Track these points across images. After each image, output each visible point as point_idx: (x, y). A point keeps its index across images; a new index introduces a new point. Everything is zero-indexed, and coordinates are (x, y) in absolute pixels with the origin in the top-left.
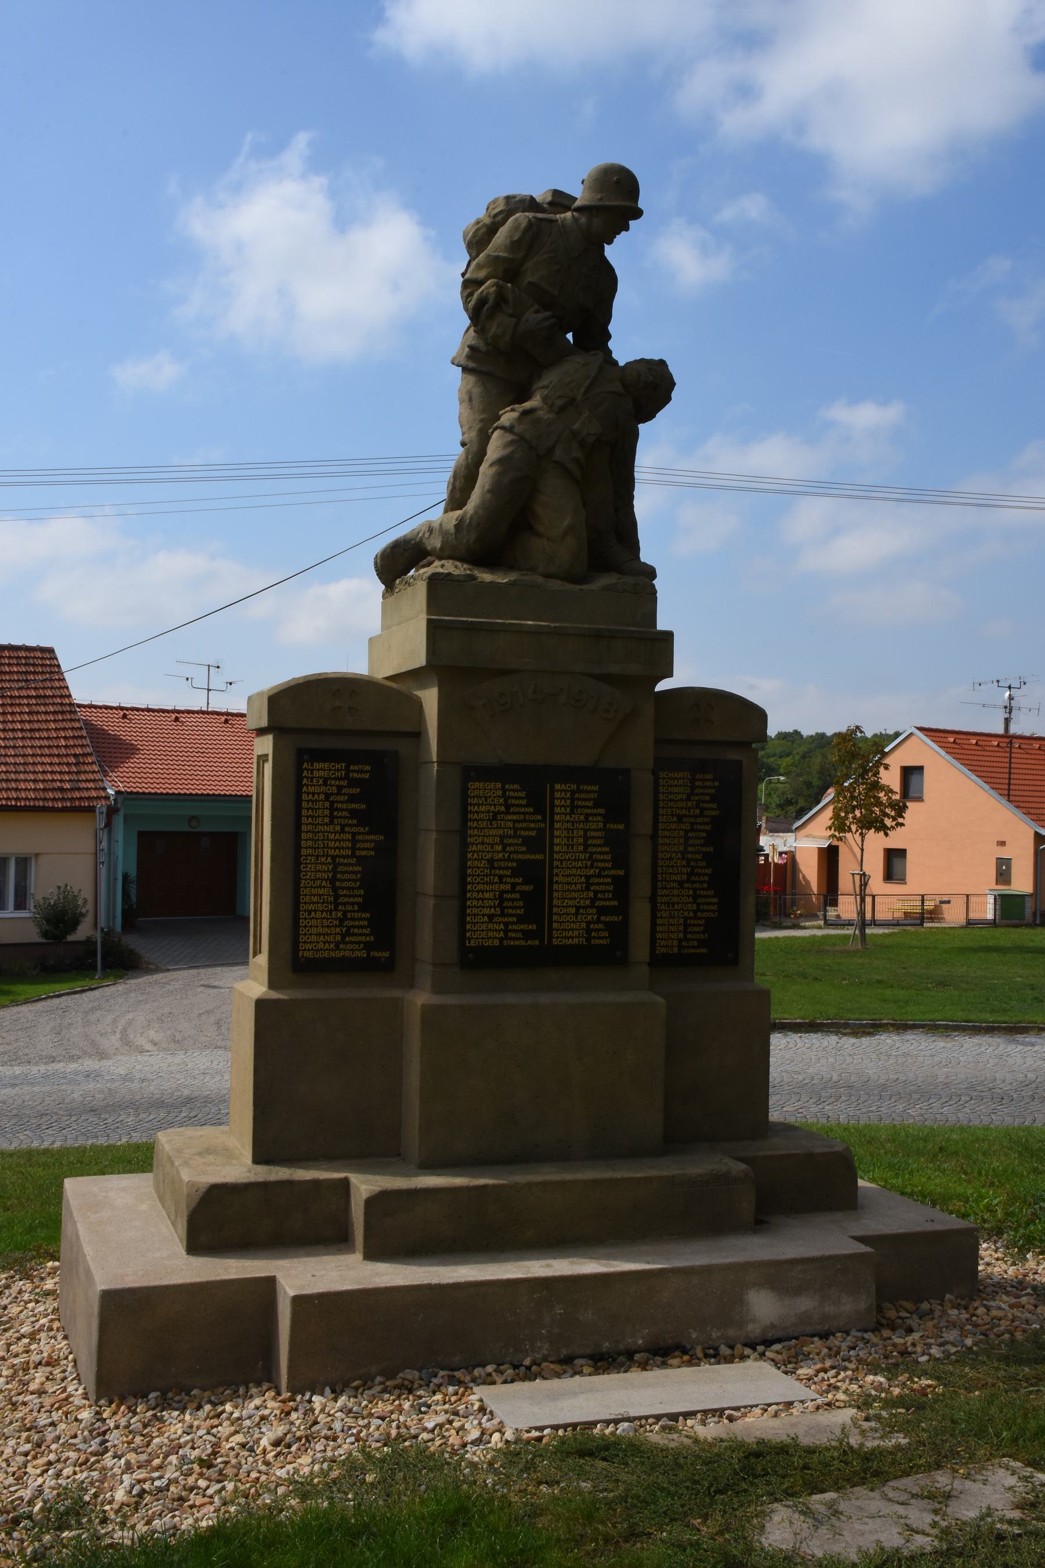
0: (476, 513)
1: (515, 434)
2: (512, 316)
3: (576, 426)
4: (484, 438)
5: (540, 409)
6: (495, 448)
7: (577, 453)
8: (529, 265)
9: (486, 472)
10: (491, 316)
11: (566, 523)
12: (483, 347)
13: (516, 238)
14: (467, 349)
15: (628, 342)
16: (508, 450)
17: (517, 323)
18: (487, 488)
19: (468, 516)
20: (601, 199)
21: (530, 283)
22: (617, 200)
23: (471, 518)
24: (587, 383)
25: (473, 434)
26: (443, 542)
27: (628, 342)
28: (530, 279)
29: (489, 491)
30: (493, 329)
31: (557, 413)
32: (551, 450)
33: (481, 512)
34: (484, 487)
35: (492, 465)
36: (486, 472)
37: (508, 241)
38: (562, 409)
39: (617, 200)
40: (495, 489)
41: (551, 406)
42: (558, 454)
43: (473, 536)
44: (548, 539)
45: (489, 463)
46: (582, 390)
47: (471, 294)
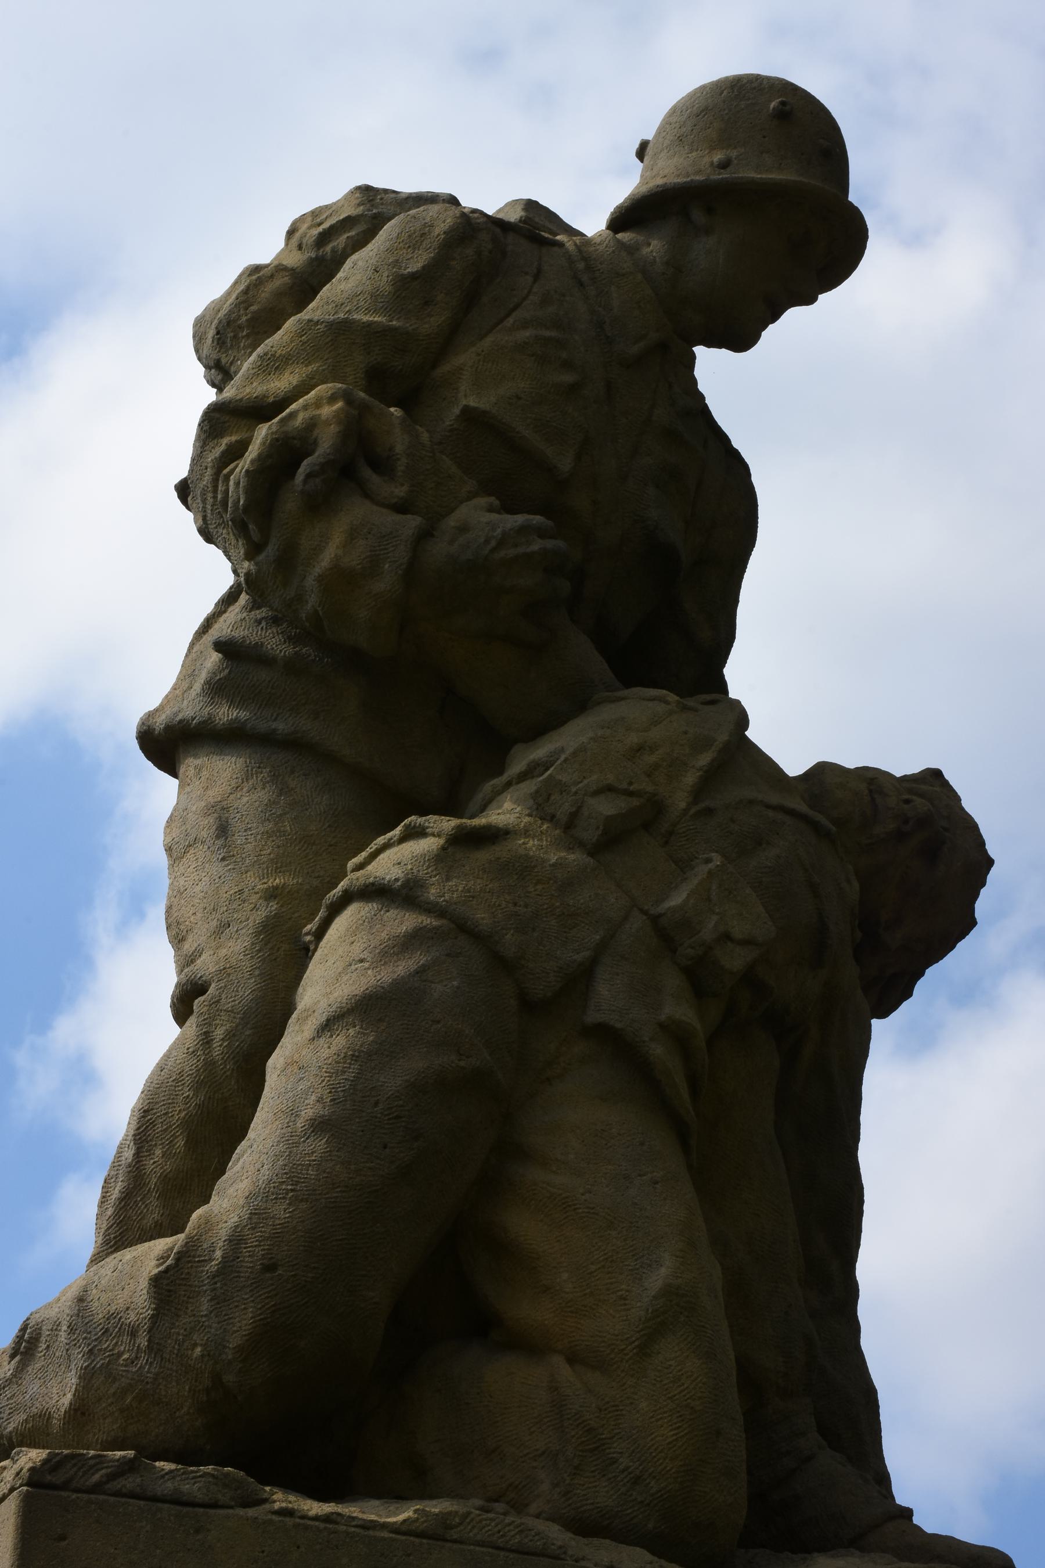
0: (257, 1216)
1: (429, 908)
2: (402, 508)
3: (676, 900)
4: (285, 955)
5: (526, 833)
6: (339, 967)
7: (678, 1008)
8: (465, 359)
9: (297, 1071)
10: (318, 506)
11: (657, 1278)
12: (274, 643)
13: (415, 265)
14: (214, 657)
15: (806, 679)
16: (402, 967)
17: (425, 535)
18: (308, 1113)
19: (223, 1232)
20: (724, 165)
21: (469, 415)
22: (763, 201)
23: (236, 1240)
24: (704, 760)
25: (237, 947)
26: (87, 1377)
27: (806, 679)
28: (472, 402)
29: (319, 1126)
30: (331, 547)
31: (595, 851)
32: (580, 979)
33: (280, 1211)
34: (293, 1113)
35: (328, 1026)
36: (297, 1071)
37: (384, 281)
38: (611, 840)
39: (763, 201)
40: (343, 1118)
41: (569, 825)
42: (610, 999)
43: (243, 1321)
44: (572, 1359)
45: (310, 1028)
46: (690, 779)
47: (235, 452)
